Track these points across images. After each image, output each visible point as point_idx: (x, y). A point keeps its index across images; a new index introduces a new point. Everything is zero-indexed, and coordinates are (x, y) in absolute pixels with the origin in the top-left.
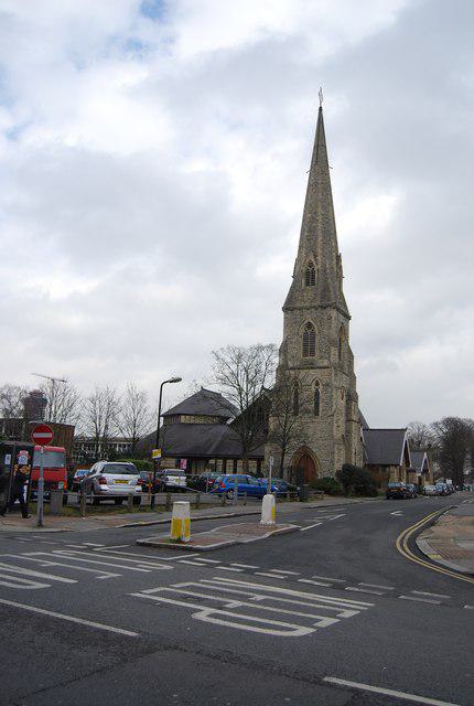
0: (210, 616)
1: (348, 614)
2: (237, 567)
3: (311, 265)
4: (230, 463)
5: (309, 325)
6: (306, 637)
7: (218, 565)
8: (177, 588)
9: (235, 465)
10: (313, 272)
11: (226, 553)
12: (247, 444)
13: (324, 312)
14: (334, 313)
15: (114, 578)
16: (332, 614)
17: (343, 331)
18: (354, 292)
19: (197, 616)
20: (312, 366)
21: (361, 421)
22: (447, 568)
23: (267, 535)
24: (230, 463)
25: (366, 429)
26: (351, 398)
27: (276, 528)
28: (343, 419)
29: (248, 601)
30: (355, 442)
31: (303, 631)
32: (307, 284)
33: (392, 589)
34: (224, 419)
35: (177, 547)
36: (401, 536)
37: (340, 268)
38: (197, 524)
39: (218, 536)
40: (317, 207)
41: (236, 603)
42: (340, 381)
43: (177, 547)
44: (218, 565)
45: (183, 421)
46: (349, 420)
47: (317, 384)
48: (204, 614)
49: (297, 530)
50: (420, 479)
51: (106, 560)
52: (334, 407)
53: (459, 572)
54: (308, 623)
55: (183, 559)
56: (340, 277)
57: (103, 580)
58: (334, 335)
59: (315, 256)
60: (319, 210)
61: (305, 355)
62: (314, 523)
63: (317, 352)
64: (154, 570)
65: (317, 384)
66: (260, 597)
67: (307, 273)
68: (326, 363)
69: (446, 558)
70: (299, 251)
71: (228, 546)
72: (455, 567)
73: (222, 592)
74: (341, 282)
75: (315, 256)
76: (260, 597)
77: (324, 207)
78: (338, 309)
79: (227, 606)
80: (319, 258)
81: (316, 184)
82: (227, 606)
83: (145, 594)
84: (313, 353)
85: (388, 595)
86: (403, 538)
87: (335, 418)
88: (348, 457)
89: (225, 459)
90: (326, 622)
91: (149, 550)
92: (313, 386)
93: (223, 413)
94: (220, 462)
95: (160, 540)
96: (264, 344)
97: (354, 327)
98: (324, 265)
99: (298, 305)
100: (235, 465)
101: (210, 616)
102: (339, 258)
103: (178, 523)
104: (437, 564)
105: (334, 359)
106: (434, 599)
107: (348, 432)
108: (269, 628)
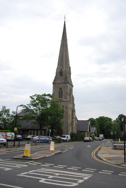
0: (45, 181)
1: (86, 178)
2: (47, 165)
3: (61, 70)
4: (36, 131)
5: (61, 88)
6: (76, 186)
7: (41, 164)
8: (31, 172)
9: (34, 132)
10: (62, 72)
11: (44, 160)
12: (41, 126)
13: (65, 84)
14: (68, 85)
15: (10, 170)
16: (82, 179)
17: (71, 90)
18: (74, 78)
19: (40, 181)
20: (62, 101)
21: (76, 118)
22: (109, 163)
23: (53, 154)
24: (36, 131)
25: (77, 121)
26: (73, 111)
27: (55, 152)
28: (71, 117)
29: (55, 176)
30: (74, 124)
31: (75, 184)
32: (60, 76)
33: (113, 172)
34: (33, 118)
35: (25, 159)
36: (93, 152)
37: (70, 71)
38: (32, 152)
39: (39, 155)
40: (63, 52)
41: (51, 177)
42: (70, 106)
43: (25, 159)
44: (41, 164)
45: (20, 118)
46: (73, 118)
47: (63, 107)
48: (42, 181)
49: (61, 153)
50: (93, 135)
51: (4, 164)
52: (68, 114)
53: (113, 164)
54: (76, 182)
55: (29, 163)
56: (70, 74)
57: (7, 171)
58: (69, 92)
59: (63, 67)
60: (64, 53)
61: (59, 98)
62: (66, 150)
63: (63, 97)
64: (40, 169)
65: (63, 107)
66: (57, 174)
67: (60, 72)
68: (66, 100)
69: (108, 160)
70: (58, 65)
71: (42, 158)
72: (111, 162)
73: (45, 173)
74: (70, 75)
75: (63, 67)
76: (57, 174)
77: (65, 52)
78: (70, 84)
79: (49, 177)
80: (64, 68)
81: (62, 44)
82: (49, 177)
83: (22, 175)
84: (62, 97)
85: (95, 171)
86: (93, 154)
87: (69, 117)
88: (72, 130)
89: (37, 130)
90: (81, 181)
91: (18, 160)
92: (62, 107)
93: (34, 115)
94: (33, 131)
95: (19, 157)
96: (46, 94)
97: (74, 89)
98: (65, 70)
99: (57, 82)
100: (34, 132)
101: (45, 181)
102: (70, 68)
103: (27, 151)
104: (106, 162)
105: (68, 99)
106: (110, 172)
107: (72, 121)
108: (62, 184)
